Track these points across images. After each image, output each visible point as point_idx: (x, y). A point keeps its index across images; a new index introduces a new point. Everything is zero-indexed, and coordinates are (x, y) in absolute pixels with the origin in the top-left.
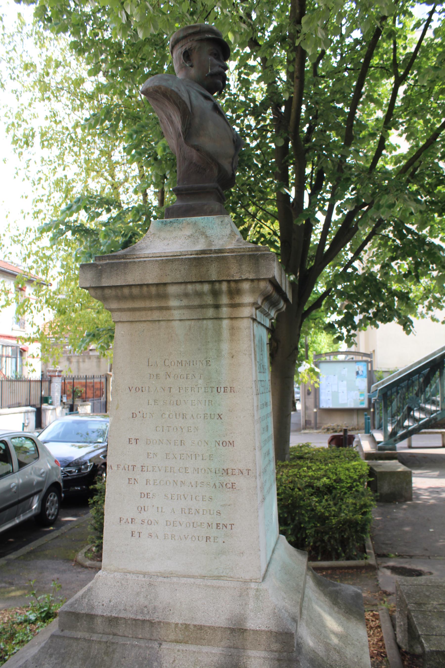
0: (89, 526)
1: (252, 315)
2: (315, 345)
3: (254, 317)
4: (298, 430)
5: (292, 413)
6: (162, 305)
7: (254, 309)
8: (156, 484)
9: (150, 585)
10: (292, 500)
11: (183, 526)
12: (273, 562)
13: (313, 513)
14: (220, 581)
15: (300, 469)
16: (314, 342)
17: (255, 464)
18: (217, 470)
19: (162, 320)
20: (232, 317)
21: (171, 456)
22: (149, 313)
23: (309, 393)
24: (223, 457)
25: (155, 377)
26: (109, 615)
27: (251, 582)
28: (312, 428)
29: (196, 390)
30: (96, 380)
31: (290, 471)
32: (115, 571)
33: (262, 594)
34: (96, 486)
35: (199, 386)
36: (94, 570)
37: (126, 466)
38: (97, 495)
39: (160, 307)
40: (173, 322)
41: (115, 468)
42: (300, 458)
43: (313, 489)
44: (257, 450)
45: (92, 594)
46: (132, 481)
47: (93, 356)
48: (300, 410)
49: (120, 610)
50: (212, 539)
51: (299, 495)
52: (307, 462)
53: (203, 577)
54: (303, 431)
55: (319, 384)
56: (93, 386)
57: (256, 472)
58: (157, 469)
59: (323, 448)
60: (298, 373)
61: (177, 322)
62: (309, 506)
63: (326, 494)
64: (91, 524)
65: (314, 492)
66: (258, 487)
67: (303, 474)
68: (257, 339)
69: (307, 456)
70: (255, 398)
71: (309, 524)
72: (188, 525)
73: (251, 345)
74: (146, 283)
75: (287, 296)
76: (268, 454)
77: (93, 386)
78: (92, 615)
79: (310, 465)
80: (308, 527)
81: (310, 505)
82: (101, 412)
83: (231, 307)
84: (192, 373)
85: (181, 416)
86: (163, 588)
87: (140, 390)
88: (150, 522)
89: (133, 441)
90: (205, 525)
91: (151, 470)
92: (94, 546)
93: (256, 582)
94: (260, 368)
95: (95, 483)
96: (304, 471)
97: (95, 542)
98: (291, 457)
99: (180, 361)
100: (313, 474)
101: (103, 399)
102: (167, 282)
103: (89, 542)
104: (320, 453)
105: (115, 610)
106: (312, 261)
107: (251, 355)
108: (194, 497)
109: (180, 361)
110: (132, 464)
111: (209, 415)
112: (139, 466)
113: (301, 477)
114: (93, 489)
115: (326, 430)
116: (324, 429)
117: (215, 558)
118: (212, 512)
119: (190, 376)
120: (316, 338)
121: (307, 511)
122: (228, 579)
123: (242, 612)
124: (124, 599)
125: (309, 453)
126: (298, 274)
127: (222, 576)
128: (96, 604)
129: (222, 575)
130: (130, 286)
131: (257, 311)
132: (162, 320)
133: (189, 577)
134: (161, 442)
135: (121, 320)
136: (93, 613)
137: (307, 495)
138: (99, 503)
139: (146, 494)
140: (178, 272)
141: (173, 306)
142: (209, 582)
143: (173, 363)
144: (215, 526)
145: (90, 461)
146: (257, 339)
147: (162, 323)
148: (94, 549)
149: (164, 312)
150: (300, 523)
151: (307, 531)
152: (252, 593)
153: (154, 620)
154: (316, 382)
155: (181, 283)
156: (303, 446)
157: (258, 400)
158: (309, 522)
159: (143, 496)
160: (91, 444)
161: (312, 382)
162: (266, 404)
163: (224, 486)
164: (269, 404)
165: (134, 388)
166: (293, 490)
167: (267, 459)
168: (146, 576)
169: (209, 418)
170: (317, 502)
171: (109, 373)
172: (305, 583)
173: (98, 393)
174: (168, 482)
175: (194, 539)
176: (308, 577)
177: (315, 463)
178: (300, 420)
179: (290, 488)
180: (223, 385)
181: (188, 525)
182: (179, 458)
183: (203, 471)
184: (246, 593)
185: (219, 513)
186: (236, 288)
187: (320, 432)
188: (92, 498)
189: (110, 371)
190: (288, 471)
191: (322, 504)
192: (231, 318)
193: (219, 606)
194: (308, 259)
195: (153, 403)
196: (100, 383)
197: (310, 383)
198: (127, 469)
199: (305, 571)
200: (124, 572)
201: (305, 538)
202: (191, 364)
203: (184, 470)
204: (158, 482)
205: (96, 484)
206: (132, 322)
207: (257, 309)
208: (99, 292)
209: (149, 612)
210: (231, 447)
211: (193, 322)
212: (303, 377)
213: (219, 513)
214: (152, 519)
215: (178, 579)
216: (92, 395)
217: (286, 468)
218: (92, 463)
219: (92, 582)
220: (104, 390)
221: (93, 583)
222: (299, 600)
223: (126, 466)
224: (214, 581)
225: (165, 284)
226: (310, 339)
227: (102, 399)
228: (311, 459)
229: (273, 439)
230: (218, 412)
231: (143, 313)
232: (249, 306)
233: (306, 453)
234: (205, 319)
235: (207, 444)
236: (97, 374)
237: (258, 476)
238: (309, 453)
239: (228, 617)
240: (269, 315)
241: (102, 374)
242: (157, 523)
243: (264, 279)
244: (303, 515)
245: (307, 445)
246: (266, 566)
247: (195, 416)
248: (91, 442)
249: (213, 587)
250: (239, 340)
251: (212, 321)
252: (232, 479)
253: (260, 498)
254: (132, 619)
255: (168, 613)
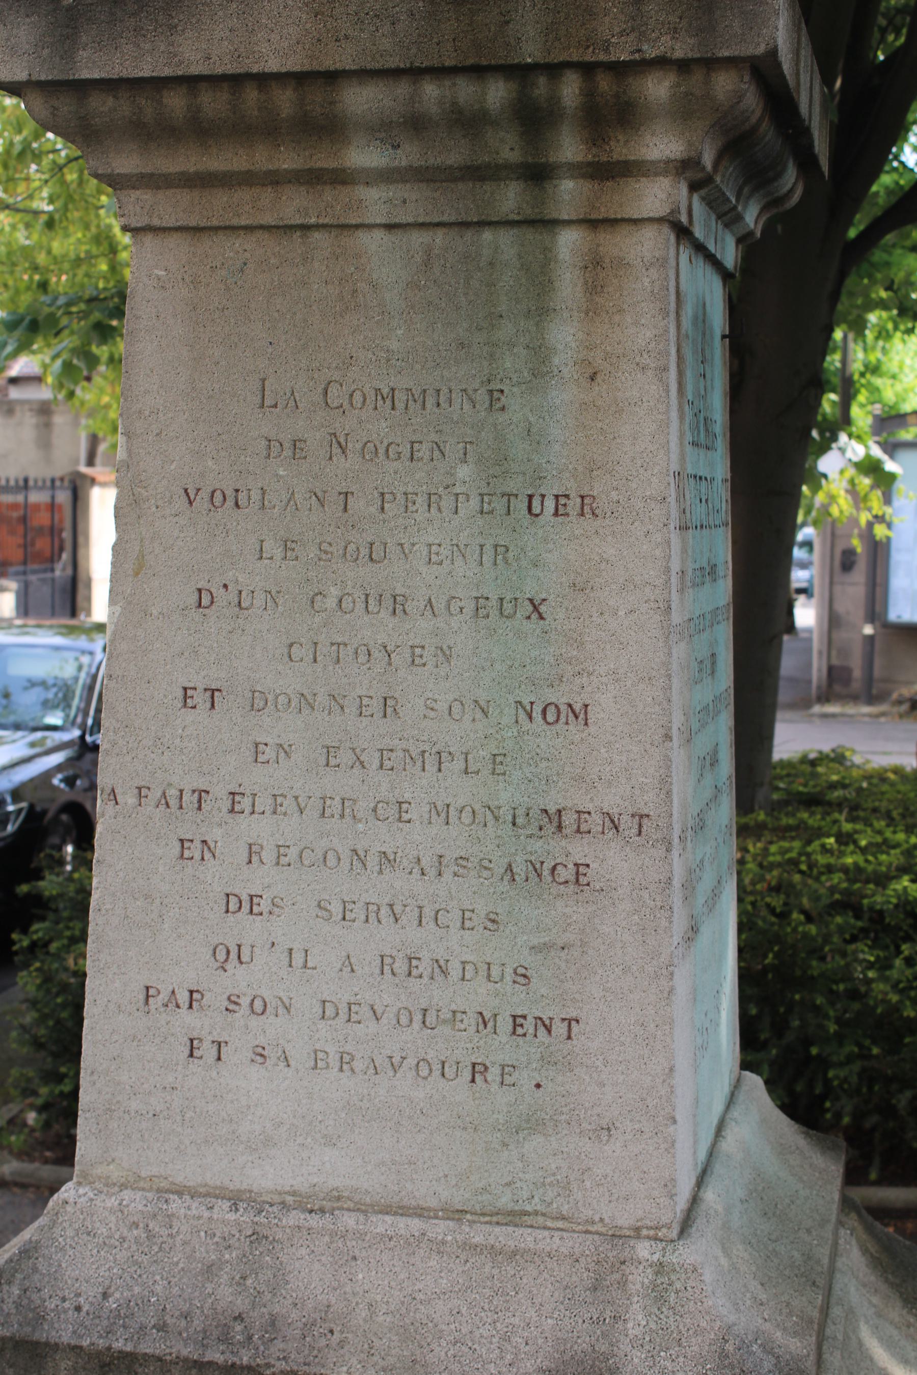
0: (14, 1034)
1: (675, 211)
2: (878, 381)
3: (684, 219)
4: (803, 704)
5: (786, 638)
6: (319, 165)
7: (684, 190)
8: (284, 860)
9: (256, 1237)
10: (776, 956)
11: (384, 1021)
12: (718, 1168)
13: (856, 1006)
14: (521, 1231)
15: (809, 842)
16: (874, 369)
17: (669, 793)
18: (521, 812)
19: (317, 227)
20: (593, 216)
21: (345, 757)
22: (267, 195)
23: (848, 561)
24: (544, 764)
25: (288, 453)
26: (102, 1343)
27: (638, 1237)
28: (854, 698)
29: (447, 503)
30: (35, 497)
31: (773, 848)
32: (123, 1186)
33: (678, 1285)
34: (41, 884)
35: (457, 490)
36: (30, 1195)
37: (173, 792)
38: (43, 919)
39: (310, 171)
40: (360, 233)
41: (128, 799)
42: (812, 801)
43: (858, 917)
44: (676, 742)
45: (35, 1270)
46: (195, 850)
47: (22, 402)
48: (809, 631)
49: (142, 1328)
50: (494, 1074)
51: (805, 935)
52: (836, 815)
53: (457, 1214)
54: (817, 709)
55: (889, 526)
56: (24, 520)
57: (670, 826)
58: (288, 804)
59: (897, 771)
60: (817, 479)
61: (378, 234)
62: (842, 980)
63: (907, 938)
64: (23, 1027)
65: (862, 930)
66: (677, 883)
67: (822, 860)
68: (688, 310)
69: (838, 793)
70: (675, 539)
71: (841, 1045)
72: (404, 1020)
73: (667, 331)
74: (255, 69)
75: (811, 146)
76: (714, 762)
77: (24, 520)
78: (37, 1344)
79: (847, 827)
80: (835, 1059)
81: (847, 977)
82: (53, 614)
83: (592, 177)
84: (434, 437)
85: (388, 602)
86: (303, 1251)
87: (230, 503)
88: (258, 1005)
89: (200, 698)
90: (471, 1020)
91: (268, 809)
92: (32, 1107)
93: (656, 1239)
94: (695, 428)
95: (38, 875)
96: (825, 849)
97: (35, 1093)
98: (775, 796)
99: (385, 391)
100: (862, 864)
101: (61, 571)
102: (339, 66)
103: (13, 1092)
104: (885, 788)
105: (124, 1327)
106: (898, 35)
107: (665, 369)
108: (428, 912)
109: (385, 391)
110: (195, 785)
111: (494, 602)
112: (220, 791)
113: (813, 872)
114: (28, 895)
115: (905, 707)
116: (899, 702)
117: (505, 1145)
118: (495, 972)
119: (423, 451)
120: (884, 351)
121: (833, 996)
122: (549, 1224)
123: (603, 1347)
124: (158, 1289)
125: (844, 786)
126: (838, 83)
127: (526, 1213)
128: (51, 1305)
129: (528, 1208)
130: (191, 82)
131: (696, 198)
132: (317, 227)
133: (403, 1211)
134: (306, 701)
135: (156, 222)
136: (41, 1336)
137: (835, 939)
138: (54, 947)
139: (245, 898)
140: (387, 28)
141: (364, 170)
142: (479, 1235)
143: (358, 397)
144: (505, 1024)
145: (17, 794)
146: (688, 310)
147: (317, 236)
148: (31, 1117)
149: (328, 194)
150: (808, 1042)
151: (831, 1074)
152: (639, 1278)
153: (268, 1365)
154: (880, 519)
155: (395, 73)
156: (822, 758)
157: (684, 550)
158: (840, 1038)
159: (233, 906)
160: (20, 734)
161: (864, 518)
162: (713, 571)
163: (546, 873)
164: (721, 571)
165: (205, 494)
166: (783, 916)
167: (708, 780)
168: (242, 1205)
169: (494, 613)
170: (871, 966)
171: (83, 469)
172: (834, 1255)
173: (42, 544)
174: (330, 855)
175: (424, 1072)
176: (844, 1233)
177: (867, 823)
178: (809, 665)
179: (772, 911)
180: (551, 489)
181: (404, 1020)
182: (377, 762)
183: (466, 817)
184: (617, 1276)
185: (523, 976)
186: (617, 96)
187: (883, 714)
188: (25, 931)
189: (91, 462)
190: (765, 851)
191: (894, 974)
192: (593, 224)
193: (516, 1321)
194: (882, 22)
195: (278, 553)
196: (52, 507)
197: (854, 521)
198: (173, 802)
199: (835, 1207)
200: (159, 1190)
201: (823, 1097)
202: (430, 402)
203: (393, 811)
204: (293, 852)
205: (42, 878)
206: (197, 230)
207: (694, 187)
208: (66, 106)
209: (250, 1338)
210: (574, 729)
211: (439, 237)
212: (832, 498)
213: (523, 976)
214: (267, 995)
215: (362, 1218)
216: (19, 554)
217: (759, 838)
218: (24, 805)
219: (36, 1224)
220: (67, 535)
221: (41, 1229)
222: (816, 1314)
223: (173, 792)
224: (497, 1229)
225: (332, 77)
226: (860, 355)
227: (58, 567)
228: (854, 809)
229: (732, 708)
230: (530, 589)
231: (243, 195)
232: (665, 173)
233: (833, 786)
234: (490, 224)
235: (485, 713)
236: (37, 471)
237: (676, 840)
238: (844, 786)
239: (546, 1364)
240: (739, 218)
241: (58, 474)
242: (288, 1009)
243: (732, 62)
244: (817, 1009)
245: (838, 758)
246: (693, 1181)
247: (440, 606)
248: (17, 727)
249: (494, 1252)
250: (621, 311)
251: (515, 231)
252: (579, 850)
253: (680, 925)
254: (186, 1360)
255: (323, 1342)
